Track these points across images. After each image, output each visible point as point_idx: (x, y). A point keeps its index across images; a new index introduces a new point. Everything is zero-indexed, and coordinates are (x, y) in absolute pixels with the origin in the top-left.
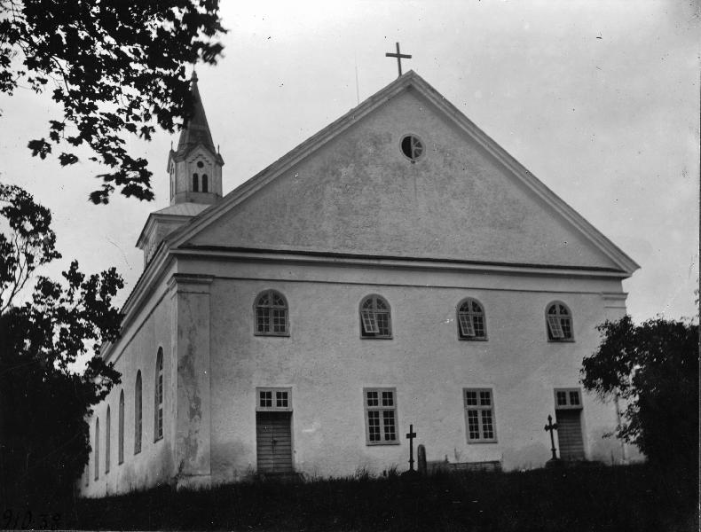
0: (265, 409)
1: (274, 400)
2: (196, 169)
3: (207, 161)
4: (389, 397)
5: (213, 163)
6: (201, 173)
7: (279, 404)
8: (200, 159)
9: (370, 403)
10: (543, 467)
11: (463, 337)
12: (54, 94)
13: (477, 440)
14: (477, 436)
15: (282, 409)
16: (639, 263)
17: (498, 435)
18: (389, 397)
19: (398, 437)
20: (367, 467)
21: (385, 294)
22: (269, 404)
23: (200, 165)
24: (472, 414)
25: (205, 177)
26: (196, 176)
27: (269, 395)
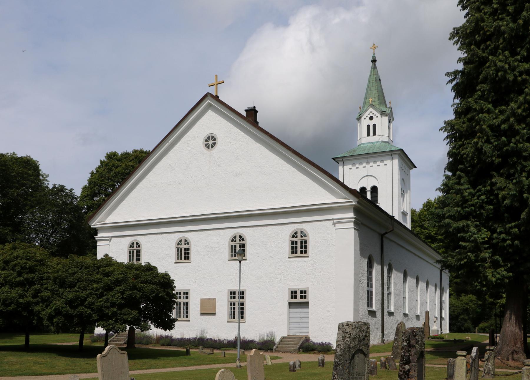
0: (294, 300)
1: (298, 295)
3: (375, 115)
5: (379, 116)
6: (371, 123)
8: (371, 115)
9: (231, 298)
10: (360, 354)
12: (88, 179)
15: (303, 300)
16: (332, 159)
21: (188, 236)
22: (296, 297)
23: (371, 118)
24: (232, 305)
25: (374, 126)
27: (296, 292)
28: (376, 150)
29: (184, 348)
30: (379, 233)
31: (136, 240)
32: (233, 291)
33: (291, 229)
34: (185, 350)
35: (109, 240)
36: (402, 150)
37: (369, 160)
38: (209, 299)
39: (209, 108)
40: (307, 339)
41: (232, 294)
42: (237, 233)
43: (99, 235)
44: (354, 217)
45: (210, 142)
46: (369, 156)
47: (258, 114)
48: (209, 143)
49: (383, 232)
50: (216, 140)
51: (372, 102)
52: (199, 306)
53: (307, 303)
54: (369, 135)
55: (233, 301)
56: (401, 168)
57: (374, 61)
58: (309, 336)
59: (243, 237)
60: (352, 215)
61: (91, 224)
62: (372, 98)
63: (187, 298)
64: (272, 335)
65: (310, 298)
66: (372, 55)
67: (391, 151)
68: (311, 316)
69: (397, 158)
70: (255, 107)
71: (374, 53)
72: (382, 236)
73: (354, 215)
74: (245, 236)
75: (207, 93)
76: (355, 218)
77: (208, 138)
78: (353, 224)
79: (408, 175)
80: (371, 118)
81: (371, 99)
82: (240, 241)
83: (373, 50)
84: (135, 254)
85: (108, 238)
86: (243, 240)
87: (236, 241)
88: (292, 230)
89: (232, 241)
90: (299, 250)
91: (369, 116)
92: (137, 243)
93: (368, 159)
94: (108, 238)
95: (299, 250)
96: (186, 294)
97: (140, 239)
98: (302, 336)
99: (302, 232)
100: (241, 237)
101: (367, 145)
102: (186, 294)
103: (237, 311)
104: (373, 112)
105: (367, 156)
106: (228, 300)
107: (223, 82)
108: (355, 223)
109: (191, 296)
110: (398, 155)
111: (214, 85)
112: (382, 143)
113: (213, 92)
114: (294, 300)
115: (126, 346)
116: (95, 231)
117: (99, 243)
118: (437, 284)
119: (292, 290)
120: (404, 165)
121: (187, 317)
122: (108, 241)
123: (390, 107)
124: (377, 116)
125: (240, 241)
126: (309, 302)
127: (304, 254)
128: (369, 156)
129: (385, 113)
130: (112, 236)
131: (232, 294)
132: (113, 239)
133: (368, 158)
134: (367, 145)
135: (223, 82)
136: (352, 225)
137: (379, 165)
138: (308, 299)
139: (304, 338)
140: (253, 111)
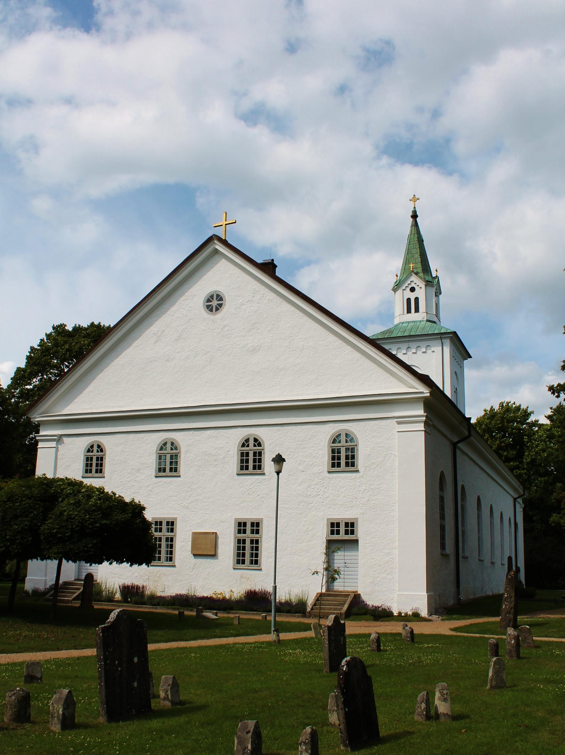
0: (335, 537)
1: (342, 529)
2: (408, 294)
3: (418, 286)
4: (256, 526)
6: (412, 296)
7: (347, 533)
11: (235, 519)
13: (164, 474)
14: (91, 472)
17: (82, 458)
18: (256, 526)
19: (176, 530)
20: (299, 598)
22: (338, 533)
25: (417, 299)
26: (409, 300)
28: (420, 332)
29: (174, 609)
30: (451, 442)
31: (97, 441)
32: (335, 522)
33: (332, 429)
34: (177, 612)
35: (57, 440)
36: (455, 333)
37: (411, 344)
38: (206, 533)
39: (215, 255)
40: (357, 597)
41: (241, 526)
42: (250, 435)
43: (42, 433)
44: (425, 414)
45: (215, 303)
46: (410, 339)
47: (277, 269)
48: (213, 305)
49: (455, 440)
50: (222, 300)
51: (413, 268)
52: (190, 543)
53: (356, 542)
54: (409, 311)
55: (242, 536)
56: (453, 357)
57: (415, 216)
58: (359, 592)
59: (260, 440)
60: (421, 412)
61: (31, 416)
62: (413, 264)
63: (172, 531)
64: (273, 586)
65: (361, 533)
66: (413, 209)
67: (440, 333)
68: (361, 562)
69: (449, 344)
70: (273, 260)
71: (415, 206)
72: (454, 445)
73: (424, 413)
74: (261, 439)
75: (213, 235)
76: (426, 417)
77: (212, 297)
78: (423, 424)
79: (462, 367)
80: (413, 290)
81: (411, 265)
82: (255, 446)
83: (413, 203)
84: (94, 462)
85: (56, 438)
86: (260, 445)
87: (248, 446)
88: (334, 431)
89: (243, 445)
90: (343, 461)
91: (410, 287)
92: (99, 446)
93: (409, 343)
94: (56, 438)
95: (343, 461)
96: (171, 525)
97: (103, 440)
98: (348, 592)
99: (347, 435)
100: (256, 440)
101: (407, 325)
102: (171, 525)
103: (248, 552)
104: (415, 282)
105: (408, 339)
106: (235, 535)
107: (235, 223)
108: (426, 423)
109: (179, 528)
110: (450, 339)
111: (222, 225)
112: (428, 323)
113: (220, 233)
114: (335, 537)
115: (78, 605)
116: (36, 428)
117: (40, 445)
118: (511, 518)
119: (241, 521)
120: (457, 353)
121: (171, 559)
122: (55, 442)
123: (437, 276)
124: (420, 286)
125: (255, 446)
126: (358, 540)
127: (350, 467)
128: (410, 339)
129: (431, 283)
130: (62, 435)
131: (241, 526)
132: (65, 439)
133: (409, 341)
134: (407, 325)
135: (234, 221)
136: (421, 427)
137: (433, 352)
138: (357, 536)
139: (353, 595)
140: (271, 266)
